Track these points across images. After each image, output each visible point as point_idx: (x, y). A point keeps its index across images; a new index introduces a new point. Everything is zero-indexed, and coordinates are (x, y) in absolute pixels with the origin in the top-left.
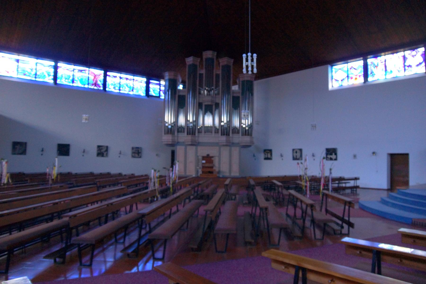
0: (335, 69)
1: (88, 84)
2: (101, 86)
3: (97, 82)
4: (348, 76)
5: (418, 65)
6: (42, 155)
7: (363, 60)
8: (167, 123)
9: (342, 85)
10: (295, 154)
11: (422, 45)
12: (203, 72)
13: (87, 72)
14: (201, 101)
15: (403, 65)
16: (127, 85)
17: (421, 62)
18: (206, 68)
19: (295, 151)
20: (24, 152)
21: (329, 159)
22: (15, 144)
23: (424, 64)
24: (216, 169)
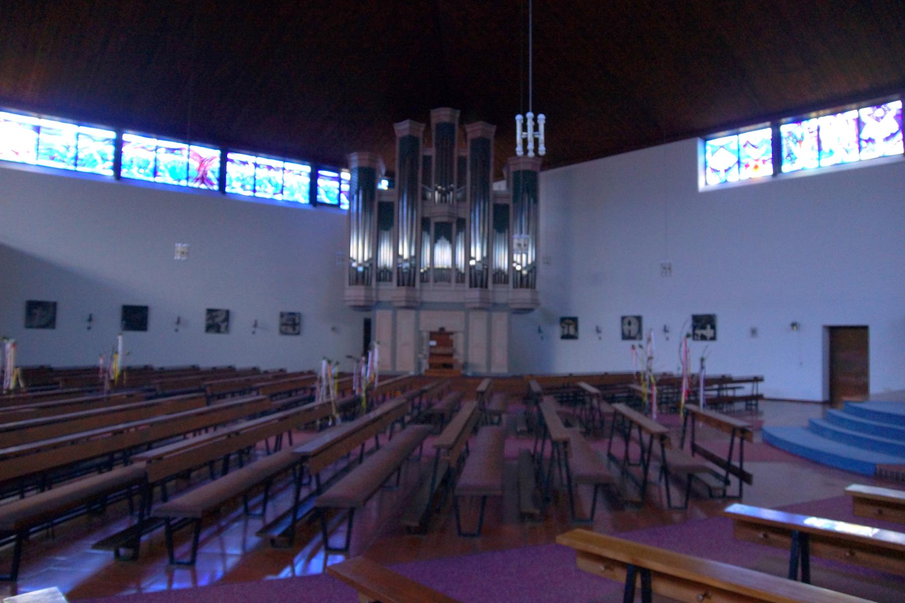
0: (712, 146)
1: (188, 179)
2: (215, 182)
3: (205, 173)
4: (739, 162)
5: (887, 139)
6: (89, 328)
7: (772, 126)
8: (354, 261)
9: (726, 181)
10: (626, 327)
11: (896, 96)
12: (432, 152)
13: (185, 153)
14: (426, 215)
15: (856, 139)
16: (270, 181)
17: (894, 132)
18: (437, 145)
19: (626, 321)
20: (50, 323)
21: (699, 338)
22: (32, 307)
23: (900, 136)
24: (459, 358)
